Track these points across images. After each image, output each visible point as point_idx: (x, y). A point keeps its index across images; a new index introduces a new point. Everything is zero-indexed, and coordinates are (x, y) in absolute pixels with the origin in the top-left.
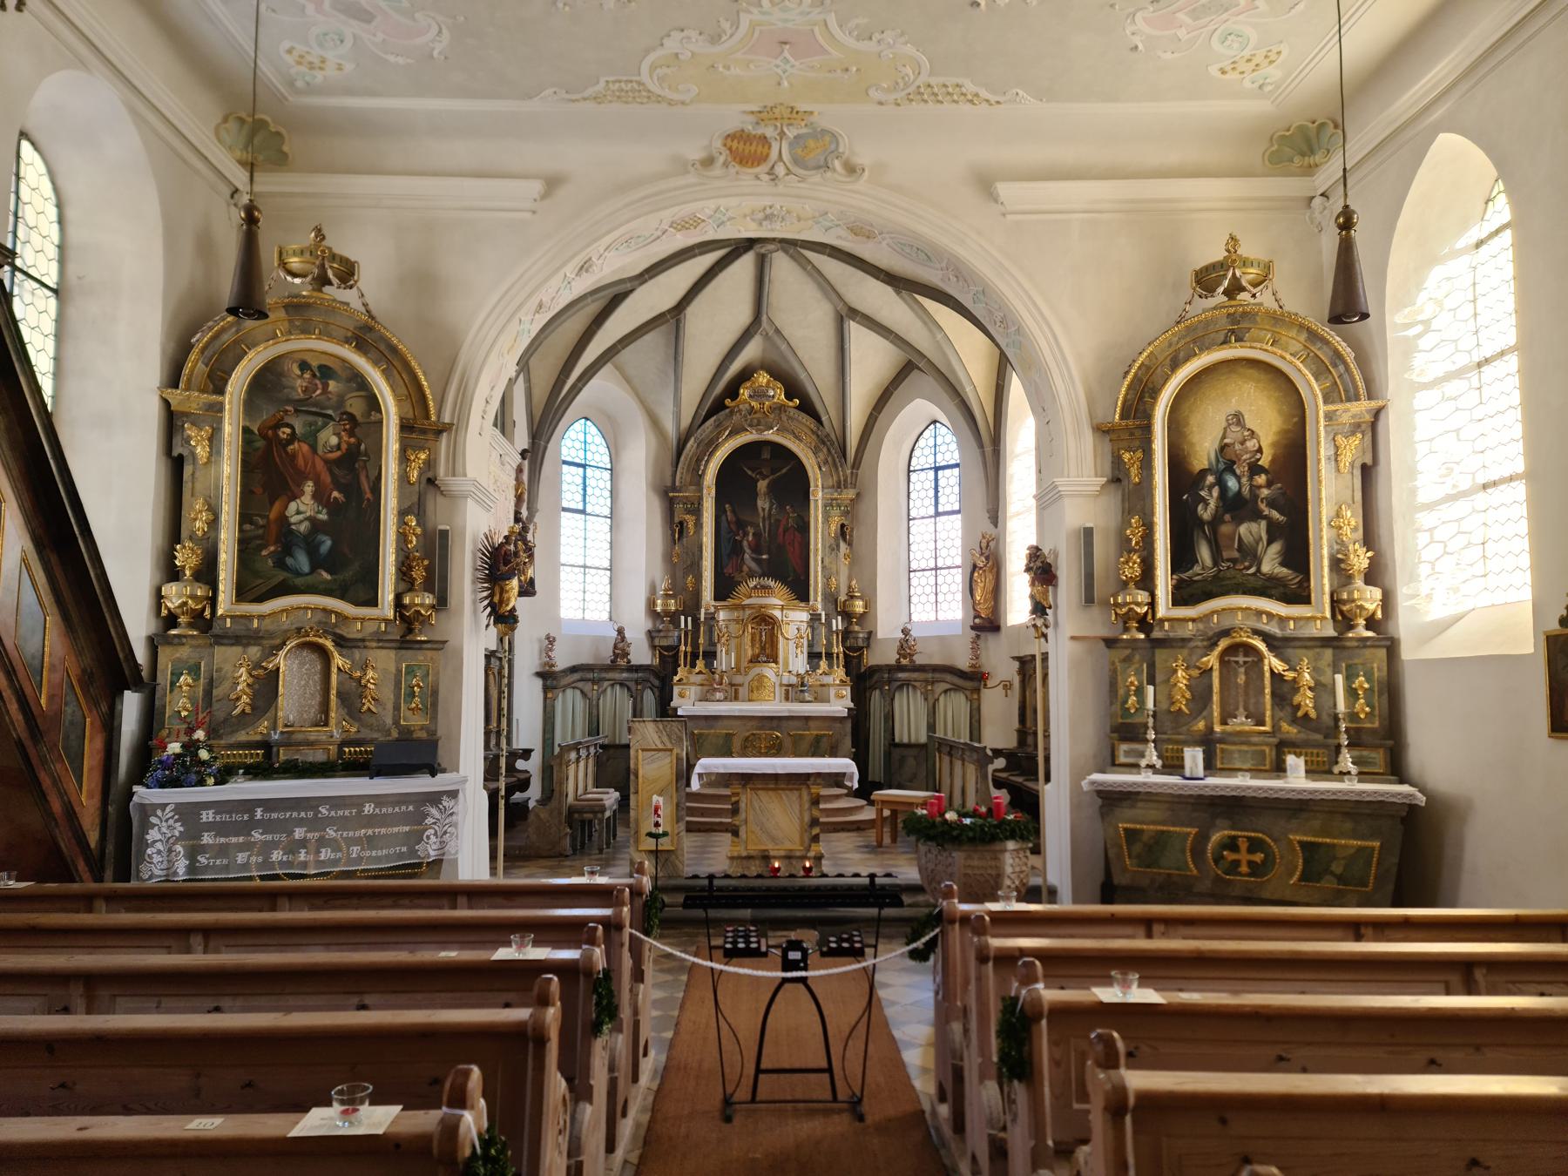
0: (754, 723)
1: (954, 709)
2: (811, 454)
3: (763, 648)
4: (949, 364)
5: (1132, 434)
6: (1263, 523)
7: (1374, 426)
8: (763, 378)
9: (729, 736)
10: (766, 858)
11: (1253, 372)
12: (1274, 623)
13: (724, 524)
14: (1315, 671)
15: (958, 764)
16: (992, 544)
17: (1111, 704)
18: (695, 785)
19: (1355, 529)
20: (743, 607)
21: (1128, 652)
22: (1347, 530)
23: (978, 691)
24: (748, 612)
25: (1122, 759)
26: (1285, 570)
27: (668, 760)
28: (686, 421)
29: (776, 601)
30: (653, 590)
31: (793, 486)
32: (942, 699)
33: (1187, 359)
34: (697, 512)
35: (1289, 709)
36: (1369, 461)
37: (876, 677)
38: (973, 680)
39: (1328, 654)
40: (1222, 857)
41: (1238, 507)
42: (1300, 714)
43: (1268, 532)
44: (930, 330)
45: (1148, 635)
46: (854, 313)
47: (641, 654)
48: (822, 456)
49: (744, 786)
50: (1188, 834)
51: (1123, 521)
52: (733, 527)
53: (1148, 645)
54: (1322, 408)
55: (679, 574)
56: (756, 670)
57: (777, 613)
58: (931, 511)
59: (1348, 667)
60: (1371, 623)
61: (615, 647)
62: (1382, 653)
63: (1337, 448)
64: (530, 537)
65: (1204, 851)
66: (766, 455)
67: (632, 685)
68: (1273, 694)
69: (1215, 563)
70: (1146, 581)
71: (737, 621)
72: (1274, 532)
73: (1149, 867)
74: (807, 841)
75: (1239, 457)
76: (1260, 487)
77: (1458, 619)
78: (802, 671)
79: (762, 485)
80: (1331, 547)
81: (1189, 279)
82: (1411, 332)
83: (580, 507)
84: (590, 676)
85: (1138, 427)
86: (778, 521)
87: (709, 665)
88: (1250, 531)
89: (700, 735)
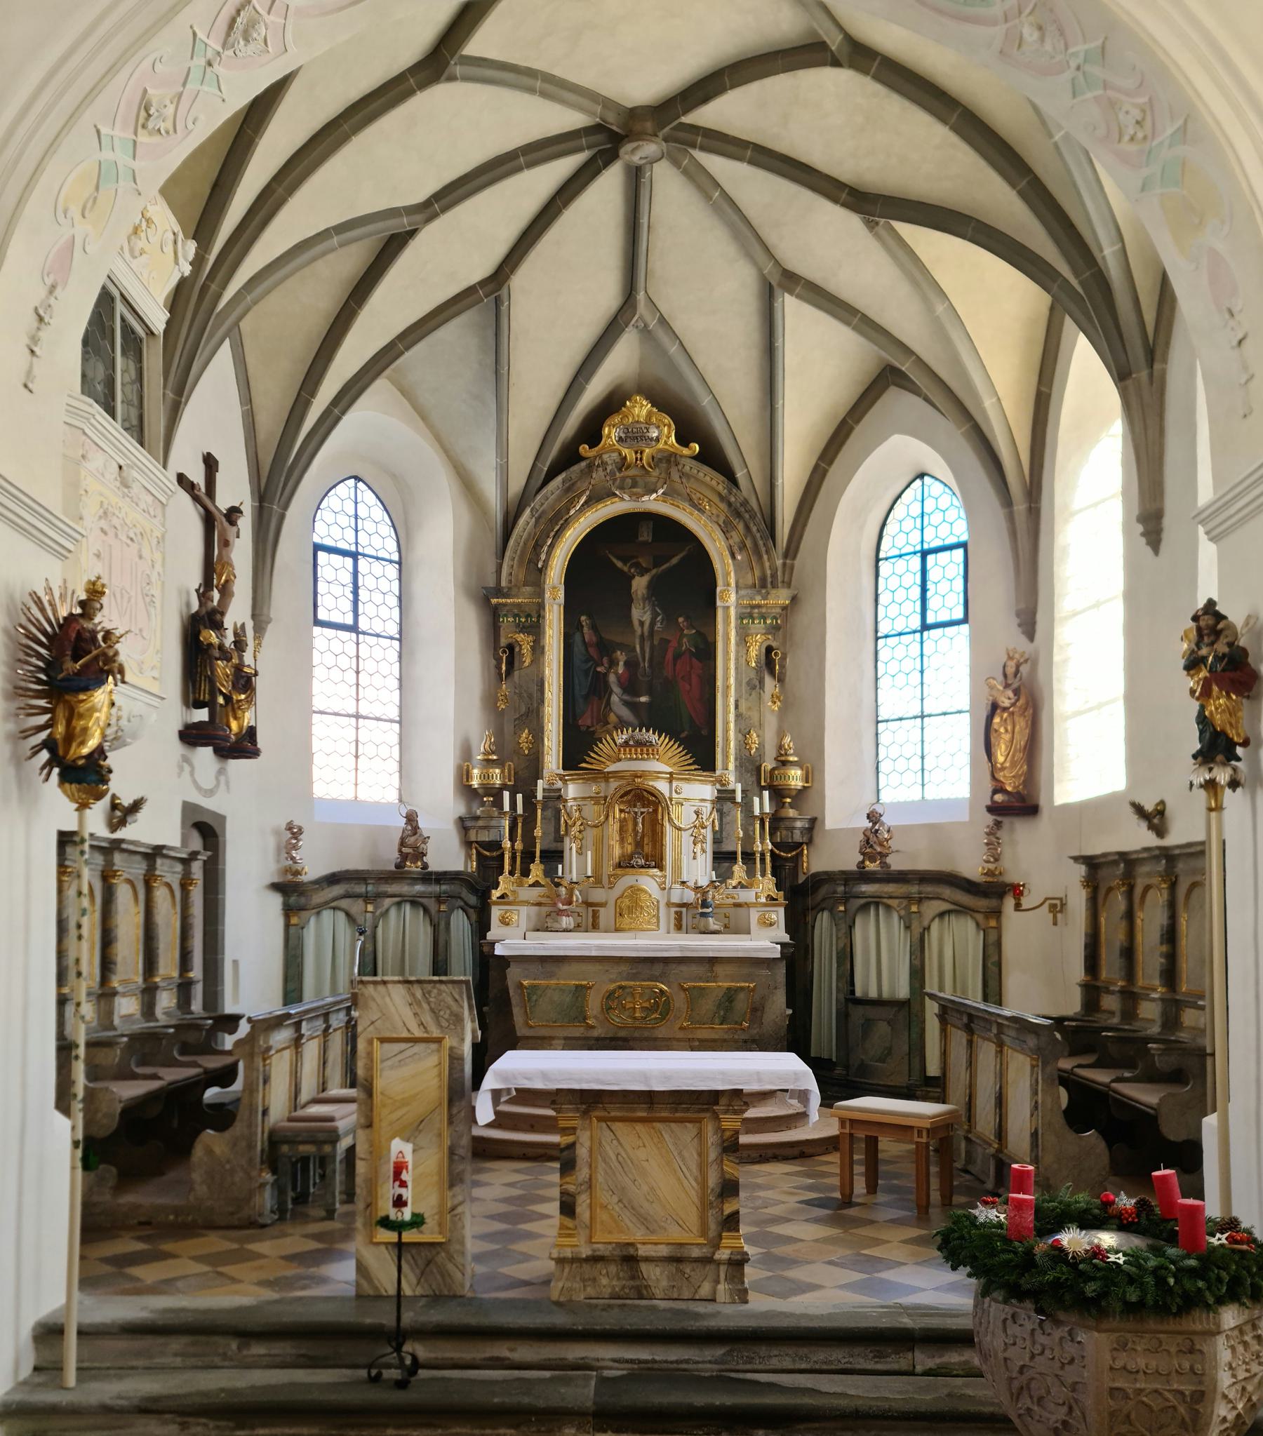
0: (624, 968)
1: (955, 942)
2: (718, 534)
3: (639, 844)
4: (956, 361)
8: (640, 409)
9: (581, 990)
10: (629, 1259)
13: (578, 648)
15: (986, 1052)
16: (1024, 669)
18: (484, 1111)
20: (607, 777)
23: (997, 913)
24: (614, 784)
27: (434, 1060)
28: (517, 483)
29: (660, 766)
30: (466, 753)
31: (690, 584)
32: (935, 926)
34: (535, 628)
37: (823, 891)
38: (989, 895)
44: (925, 299)
46: (792, 280)
47: (446, 853)
48: (736, 538)
49: (585, 1114)
52: (592, 651)
55: (509, 728)
56: (628, 880)
57: (662, 786)
58: (916, 623)
61: (402, 843)
64: (248, 658)
66: (645, 535)
67: (431, 904)
71: (596, 799)
74: (713, 1227)
78: (703, 882)
79: (640, 584)
83: (349, 620)
84: (361, 889)
86: (665, 642)
87: (550, 873)
89: (534, 988)
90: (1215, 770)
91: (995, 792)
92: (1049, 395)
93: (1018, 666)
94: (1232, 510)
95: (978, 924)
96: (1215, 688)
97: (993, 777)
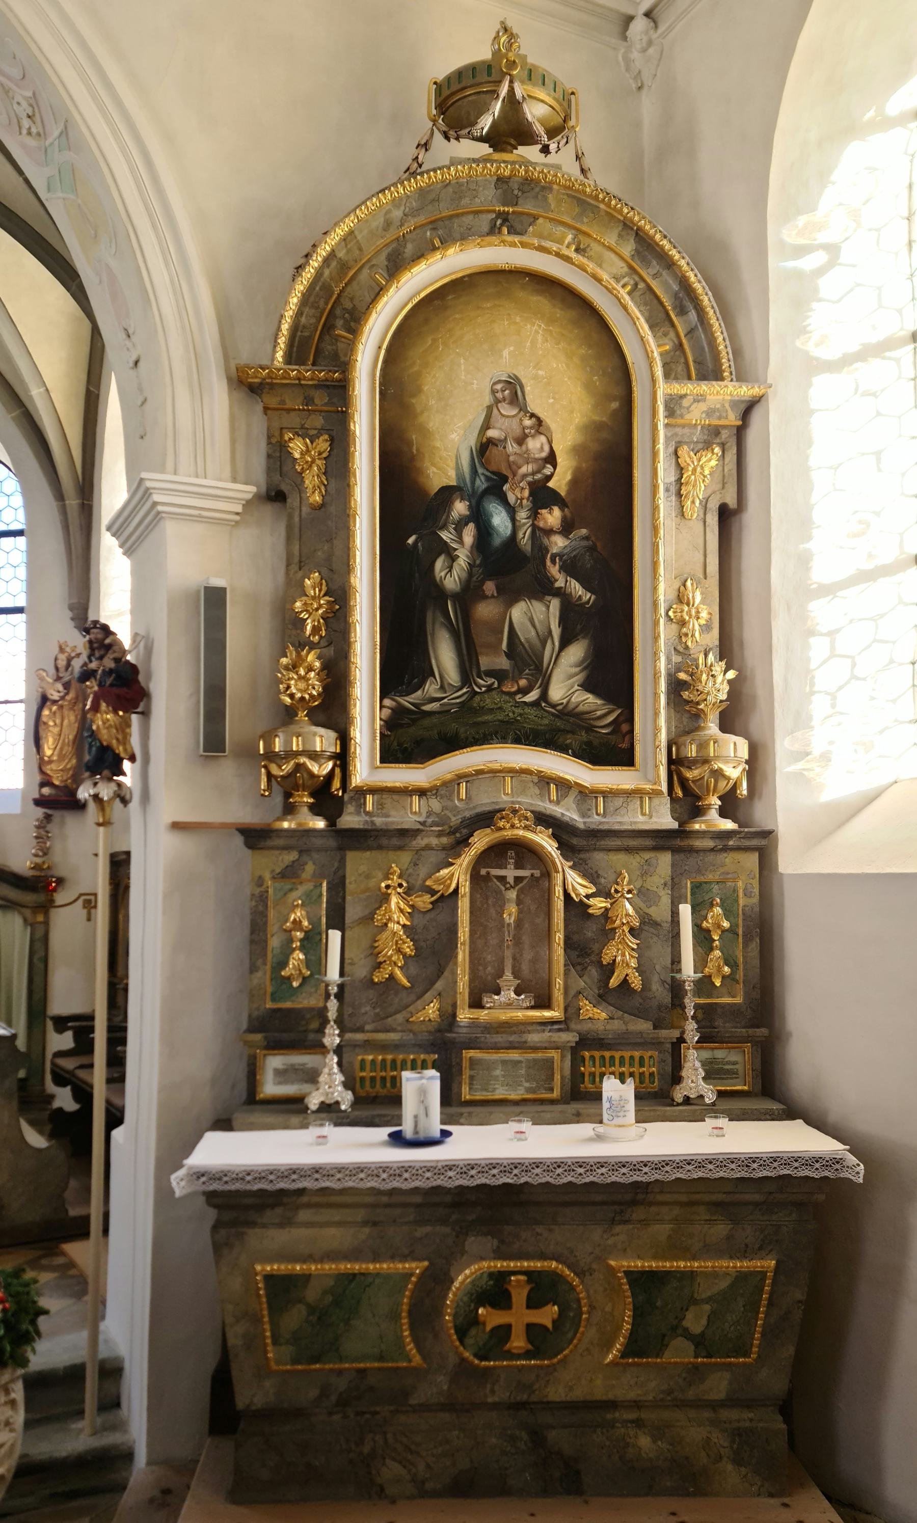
5: (308, 400)
6: (555, 604)
7: (740, 432)
11: (541, 302)
12: (570, 800)
14: (643, 894)
17: (253, 969)
19: (706, 628)
21: (293, 856)
22: (695, 626)
25: (270, 1088)
26: (590, 698)
33: (418, 257)
35: (594, 972)
36: (732, 502)
39: (665, 860)
40: (475, 1321)
41: (509, 567)
42: (614, 982)
43: (563, 621)
45: (332, 823)
50: (409, 1275)
51: (289, 582)
53: (332, 843)
54: (663, 389)
59: (697, 887)
60: (730, 805)
62: (751, 861)
63: (680, 470)
65: (438, 1311)
68: (569, 944)
69: (466, 678)
70: (332, 708)
72: (573, 622)
73: (316, 1359)
75: (513, 467)
76: (549, 532)
77: (871, 798)
80: (669, 660)
81: (423, 106)
82: (809, 263)
85: (322, 385)
88: (533, 617)
90: (99, 785)
91: (42, 785)
92: (98, 396)
93: (69, 660)
94: (131, 528)
95: (25, 920)
96: (103, 706)
97: (42, 772)
